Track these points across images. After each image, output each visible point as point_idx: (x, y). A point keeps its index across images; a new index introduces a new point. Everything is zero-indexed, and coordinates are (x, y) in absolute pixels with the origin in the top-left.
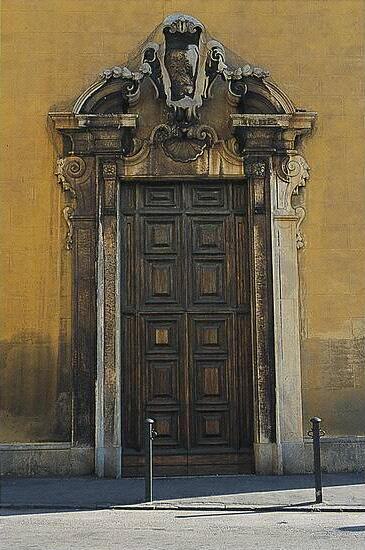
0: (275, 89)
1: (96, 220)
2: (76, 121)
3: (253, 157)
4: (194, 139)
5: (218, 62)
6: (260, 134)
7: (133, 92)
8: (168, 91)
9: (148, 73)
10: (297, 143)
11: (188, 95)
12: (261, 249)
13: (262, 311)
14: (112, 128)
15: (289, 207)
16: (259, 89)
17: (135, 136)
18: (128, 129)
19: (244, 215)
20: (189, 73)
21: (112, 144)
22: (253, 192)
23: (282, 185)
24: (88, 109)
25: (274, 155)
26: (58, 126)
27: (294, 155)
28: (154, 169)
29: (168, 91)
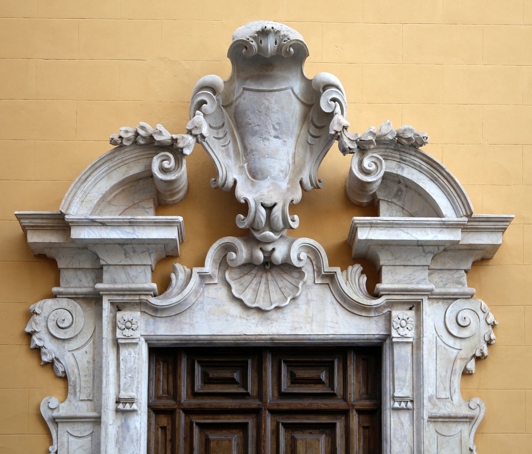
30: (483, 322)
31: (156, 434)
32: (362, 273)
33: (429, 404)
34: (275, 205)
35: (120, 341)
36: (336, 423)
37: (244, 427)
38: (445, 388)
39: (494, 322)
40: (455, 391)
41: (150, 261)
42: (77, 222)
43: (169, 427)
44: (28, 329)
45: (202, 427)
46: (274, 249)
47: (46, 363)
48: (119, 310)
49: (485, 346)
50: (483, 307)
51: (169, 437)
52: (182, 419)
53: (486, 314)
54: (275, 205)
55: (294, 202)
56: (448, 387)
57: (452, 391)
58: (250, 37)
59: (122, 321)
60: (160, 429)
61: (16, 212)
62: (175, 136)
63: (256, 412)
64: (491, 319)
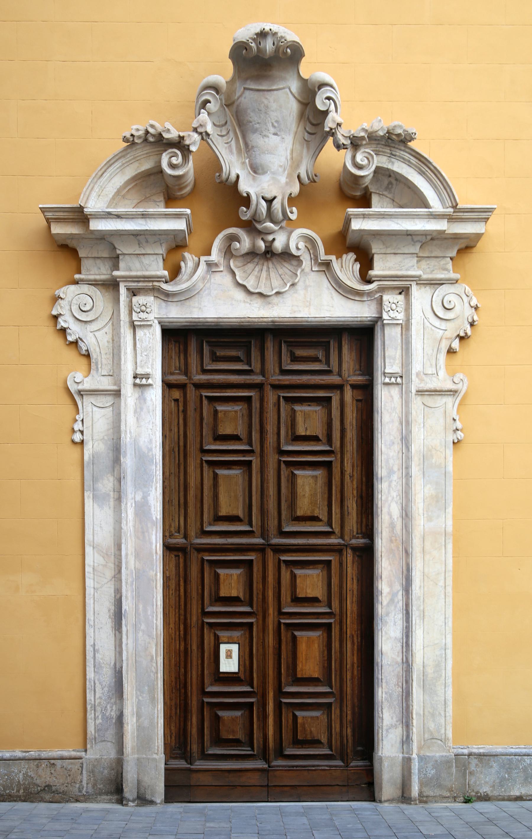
30: (467, 305)
33: (417, 379)
34: (275, 198)
35: (136, 323)
40: (440, 368)
44: (54, 313)
47: (71, 343)
48: (134, 295)
50: (466, 291)
51: (181, 408)
53: (469, 298)
54: (275, 198)
55: (293, 195)
57: (438, 367)
60: (173, 401)
61: (41, 206)
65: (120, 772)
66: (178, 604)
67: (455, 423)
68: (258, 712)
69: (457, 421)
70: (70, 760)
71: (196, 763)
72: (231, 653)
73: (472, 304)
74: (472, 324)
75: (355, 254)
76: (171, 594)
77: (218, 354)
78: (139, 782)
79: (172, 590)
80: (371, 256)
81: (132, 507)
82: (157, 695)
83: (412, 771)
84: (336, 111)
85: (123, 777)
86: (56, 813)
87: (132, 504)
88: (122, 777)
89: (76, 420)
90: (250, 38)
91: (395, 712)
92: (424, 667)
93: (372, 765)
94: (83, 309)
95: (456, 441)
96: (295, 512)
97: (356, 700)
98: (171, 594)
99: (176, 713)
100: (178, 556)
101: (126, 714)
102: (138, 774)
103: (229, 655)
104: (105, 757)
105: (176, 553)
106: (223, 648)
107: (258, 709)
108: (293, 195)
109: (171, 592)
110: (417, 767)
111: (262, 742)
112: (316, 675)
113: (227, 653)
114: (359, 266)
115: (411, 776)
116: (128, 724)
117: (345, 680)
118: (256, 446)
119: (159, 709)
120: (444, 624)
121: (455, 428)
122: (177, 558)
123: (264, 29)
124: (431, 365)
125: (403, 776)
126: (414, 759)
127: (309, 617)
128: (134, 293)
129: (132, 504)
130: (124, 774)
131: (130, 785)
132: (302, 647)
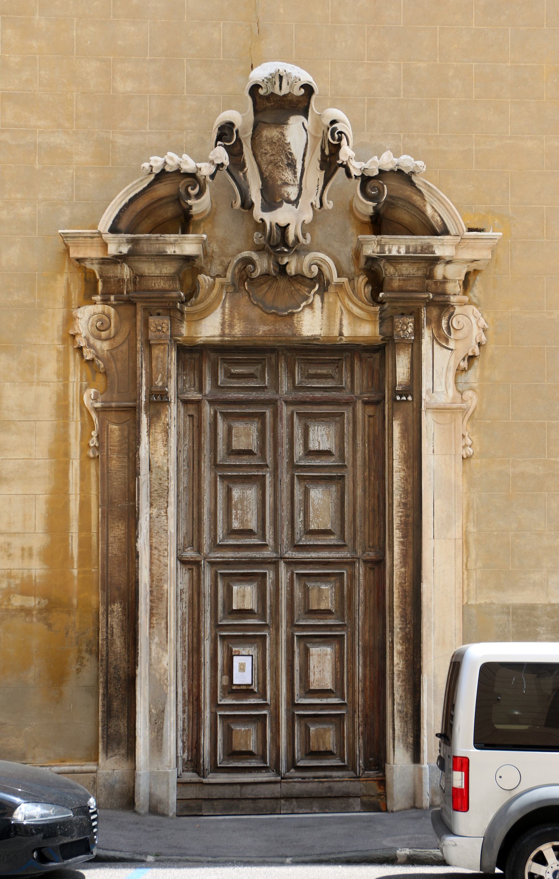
0: (351, 781)
1: (134, 410)
2: (105, 245)
3: (395, 308)
4: (299, 277)
5: (338, 147)
6: (406, 269)
7: (199, 195)
8: (256, 197)
9: (222, 165)
10: (466, 284)
11: (289, 201)
12: (405, 459)
13: (404, 556)
14: (163, 257)
15: (451, 392)
16: (408, 191)
17: (201, 271)
18: (188, 259)
19: (378, 403)
20: (292, 165)
21: (161, 284)
22: (73, 191)
23: (441, 354)
24: (122, 225)
25: (429, 304)
26: (74, 254)
27: (462, 304)
28: (231, 326)
29: (256, 197)
30: (475, 326)
31: (185, 422)
32: (367, 283)
33: (427, 397)
34: (289, 225)
35: (151, 342)
36: (265, 412)
37: (262, 416)
38: (441, 382)
39: (484, 326)
40: (450, 385)
41: (399, 860)
42: (225, 404)
43: (196, 415)
44: (71, 332)
45: (225, 415)
46: (287, 263)
47: (88, 361)
48: (151, 315)
49: (477, 346)
50: (475, 312)
51: (196, 424)
52: (207, 410)
53: (478, 319)
54: (289, 225)
55: (306, 222)
56: (443, 381)
57: (448, 385)
58: (265, 78)
59: (154, 325)
60: (188, 417)
61: (60, 231)
62: (199, 165)
63: (272, 403)
64: (482, 322)
65: (132, 786)
66: (191, 617)
67: (464, 440)
68: (271, 724)
69: (467, 437)
70: (82, 775)
71: (209, 776)
72: (244, 666)
73: (480, 325)
74: (479, 344)
75: (367, 276)
76: (184, 607)
77: (233, 371)
78: (151, 795)
79: (186, 603)
80: (381, 279)
81: (146, 521)
82: (170, 707)
83: (424, 781)
84: (348, 145)
85: (135, 790)
86: (93, 465)
87: (146, 518)
88: (134, 791)
89: (92, 436)
90: (266, 78)
91: (405, 628)
92: (434, 677)
93: (384, 776)
94: (102, 328)
95: (465, 457)
96: (309, 525)
97: (368, 683)
98: (184, 607)
99: (188, 726)
100: (192, 569)
101: (139, 727)
102: (150, 788)
103: (242, 668)
104: (117, 771)
105: (190, 567)
106: (237, 661)
107: (271, 721)
108: (306, 222)
109: (184, 605)
110: (428, 776)
111: (274, 755)
112: (329, 527)
113: (240, 666)
114: (370, 288)
115: (422, 786)
116: (140, 737)
117: (357, 628)
118: (269, 460)
119: (172, 722)
120: (454, 635)
121: (464, 444)
122: (190, 571)
123: (279, 70)
124: (441, 382)
125: (415, 786)
126: (425, 768)
127: (323, 629)
128: (149, 312)
129: (146, 518)
130: (136, 788)
131: (142, 798)
132: (313, 661)
